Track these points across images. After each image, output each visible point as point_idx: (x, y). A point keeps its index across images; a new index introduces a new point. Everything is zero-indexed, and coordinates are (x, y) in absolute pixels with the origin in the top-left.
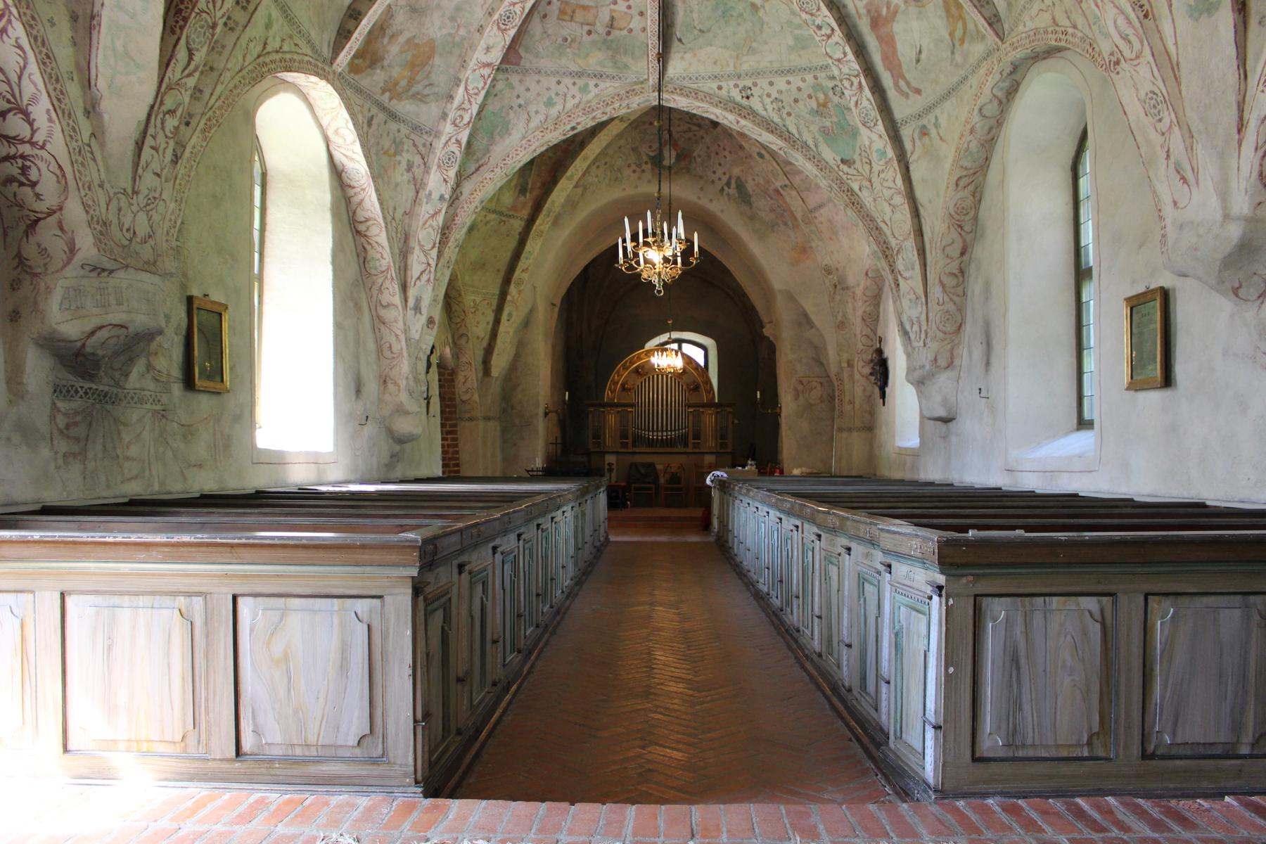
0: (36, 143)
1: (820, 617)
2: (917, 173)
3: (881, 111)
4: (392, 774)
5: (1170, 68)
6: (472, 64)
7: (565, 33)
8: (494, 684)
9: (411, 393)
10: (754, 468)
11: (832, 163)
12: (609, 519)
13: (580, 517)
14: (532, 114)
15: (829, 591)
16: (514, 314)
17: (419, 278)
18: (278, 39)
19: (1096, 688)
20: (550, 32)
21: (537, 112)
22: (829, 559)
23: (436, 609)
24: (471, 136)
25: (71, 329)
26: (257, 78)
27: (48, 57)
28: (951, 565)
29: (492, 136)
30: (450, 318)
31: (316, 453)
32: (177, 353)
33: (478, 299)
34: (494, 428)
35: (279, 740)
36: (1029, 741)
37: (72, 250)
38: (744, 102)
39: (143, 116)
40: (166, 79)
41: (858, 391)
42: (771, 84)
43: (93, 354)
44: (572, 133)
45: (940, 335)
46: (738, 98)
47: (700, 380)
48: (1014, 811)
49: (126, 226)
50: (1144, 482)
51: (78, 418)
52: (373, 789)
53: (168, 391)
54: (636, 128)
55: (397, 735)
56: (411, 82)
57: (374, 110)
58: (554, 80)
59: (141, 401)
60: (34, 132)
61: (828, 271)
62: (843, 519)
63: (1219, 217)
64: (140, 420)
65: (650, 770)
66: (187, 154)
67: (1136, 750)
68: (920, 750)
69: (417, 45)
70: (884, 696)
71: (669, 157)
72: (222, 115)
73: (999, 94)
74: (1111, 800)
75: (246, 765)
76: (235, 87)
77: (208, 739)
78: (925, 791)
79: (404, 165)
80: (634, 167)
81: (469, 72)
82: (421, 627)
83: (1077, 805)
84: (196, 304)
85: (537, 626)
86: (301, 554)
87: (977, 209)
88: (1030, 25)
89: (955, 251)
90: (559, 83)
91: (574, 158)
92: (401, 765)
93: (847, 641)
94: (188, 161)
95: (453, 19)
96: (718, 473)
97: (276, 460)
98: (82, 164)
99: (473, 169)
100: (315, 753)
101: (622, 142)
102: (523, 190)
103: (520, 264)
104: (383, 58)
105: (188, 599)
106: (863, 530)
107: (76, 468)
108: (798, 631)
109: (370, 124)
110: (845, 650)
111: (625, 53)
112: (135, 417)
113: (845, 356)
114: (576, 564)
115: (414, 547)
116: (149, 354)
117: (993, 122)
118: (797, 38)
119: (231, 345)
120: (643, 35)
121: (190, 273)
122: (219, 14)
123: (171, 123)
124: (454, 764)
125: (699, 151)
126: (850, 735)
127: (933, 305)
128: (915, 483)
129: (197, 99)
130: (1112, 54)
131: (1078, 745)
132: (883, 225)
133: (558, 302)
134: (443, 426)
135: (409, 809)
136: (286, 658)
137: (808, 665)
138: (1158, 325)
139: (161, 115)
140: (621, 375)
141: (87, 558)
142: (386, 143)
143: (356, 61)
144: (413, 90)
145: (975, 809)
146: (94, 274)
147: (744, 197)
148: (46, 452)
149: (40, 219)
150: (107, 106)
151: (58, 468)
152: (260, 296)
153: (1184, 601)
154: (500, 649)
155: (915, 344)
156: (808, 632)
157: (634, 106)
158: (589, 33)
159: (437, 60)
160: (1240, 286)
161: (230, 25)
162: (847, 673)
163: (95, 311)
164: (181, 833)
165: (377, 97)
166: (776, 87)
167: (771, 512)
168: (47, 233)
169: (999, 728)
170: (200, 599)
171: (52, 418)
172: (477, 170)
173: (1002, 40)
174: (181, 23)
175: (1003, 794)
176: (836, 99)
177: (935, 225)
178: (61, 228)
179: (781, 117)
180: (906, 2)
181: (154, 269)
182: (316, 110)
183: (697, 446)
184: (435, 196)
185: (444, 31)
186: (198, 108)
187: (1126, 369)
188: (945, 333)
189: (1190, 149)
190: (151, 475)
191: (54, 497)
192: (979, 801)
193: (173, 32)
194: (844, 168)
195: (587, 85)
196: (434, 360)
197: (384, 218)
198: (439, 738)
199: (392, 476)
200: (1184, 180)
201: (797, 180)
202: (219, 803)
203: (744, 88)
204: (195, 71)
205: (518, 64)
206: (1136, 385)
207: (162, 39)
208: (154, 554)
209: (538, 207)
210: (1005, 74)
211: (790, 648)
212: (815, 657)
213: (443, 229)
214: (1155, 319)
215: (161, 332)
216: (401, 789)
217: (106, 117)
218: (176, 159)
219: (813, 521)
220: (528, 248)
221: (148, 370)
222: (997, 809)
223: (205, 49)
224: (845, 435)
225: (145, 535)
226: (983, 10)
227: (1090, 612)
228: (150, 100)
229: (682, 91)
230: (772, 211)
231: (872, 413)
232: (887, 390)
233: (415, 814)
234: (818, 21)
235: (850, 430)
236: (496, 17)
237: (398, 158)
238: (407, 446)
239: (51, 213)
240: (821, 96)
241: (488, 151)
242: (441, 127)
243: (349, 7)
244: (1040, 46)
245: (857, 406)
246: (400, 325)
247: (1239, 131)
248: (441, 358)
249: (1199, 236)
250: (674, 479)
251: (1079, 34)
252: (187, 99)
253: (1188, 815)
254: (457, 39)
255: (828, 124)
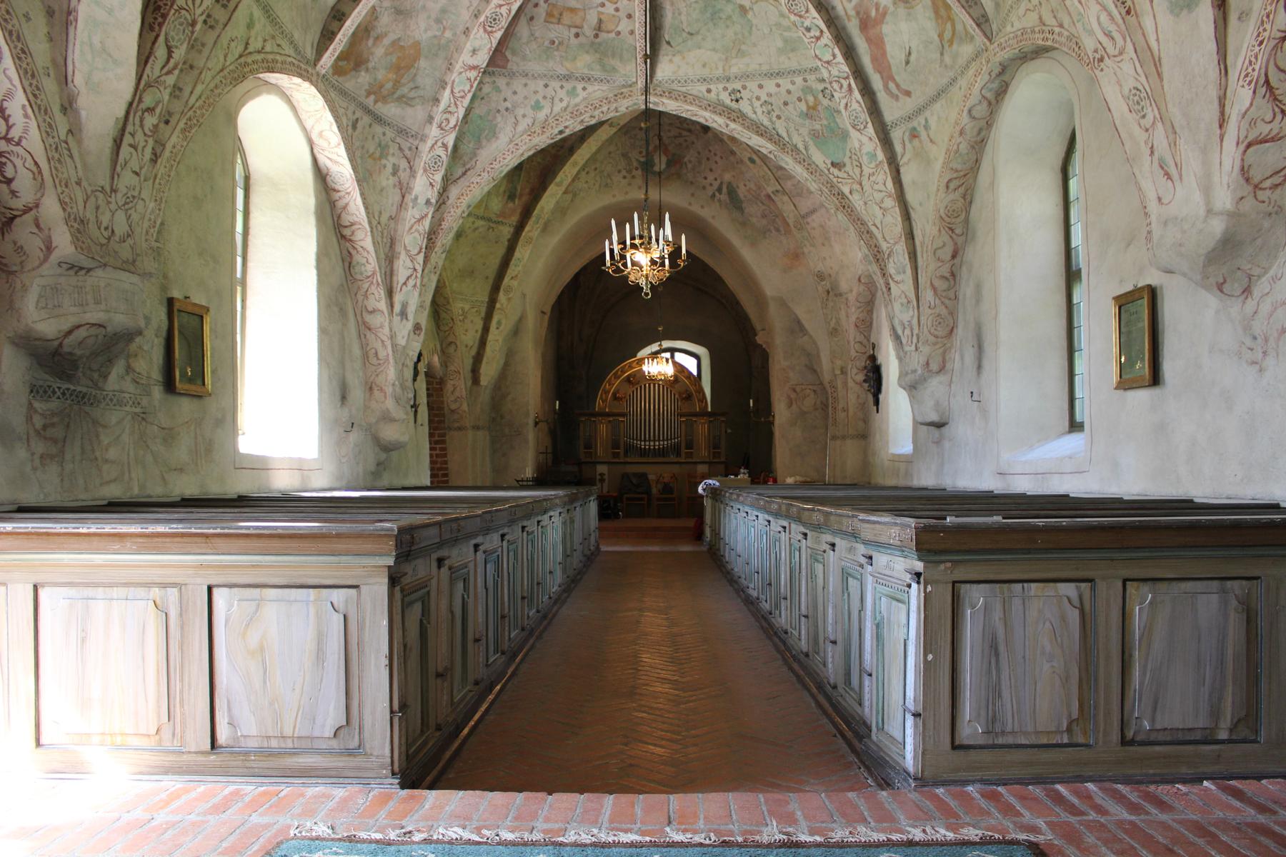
0: (12, 139)
1: (806, 617)
2: (909, 174)
3: (871, 114)
4: (369, 765)
5: (1152, 63)
6: (458, 67)
7: (552, 35)
8: (476, 683)
9: (397, 400)
10: (746, 476)
11: (822, 166)
12: (600, 529)
13: (569, 523)
14: (519, 118)
15: (815, 589)
16: (504, 322)
17: (405, 283)
18: (260, 39)
19: (1075, 672)
20: (537, 34)
21: (524, 116)
22: (815, 557)
23: (416, 600)
24: (457, 139)
25: (49, 328)
26: (238, 78)
27: (24, 52)
28: (929, 551)
29: (479, 141)
30: (438, 327)
31: (300, 460)
32: (157, 355)
33: (467, 304)
34: (483, 437)
35: (254, 732)
36: (1009, 729)
37: (49, 248)
38: (734, 105)
39: (121, 113)
40: (145, 77)
41: (852, 398)
42: (761, 87)
43: (71, 354)
44: (559, 137)
45: (932, 339)
46: (728, 102)
47: (692, 389)
48: (993, 797)
49: (104, 224)
50: (1131, 478)
51: (55, 420)
52: (350, 781)
53: (149, 394)
54: (625, 134)
55: (373, 725)
56: (397, 84)
57: (359, 114)
58: (541, 83)
59: (121, 403)
60: (9, 128)
61: (821, 276)
62: (827, 514)
63: (1202, 212)
64: (120, 422)
65: (631, 765)
66: (167, 154)
67: (1115, 736)
68: (900, 740)
69: (402, 47)
70: (867, 689)
71: (660, 163)
72: (203, 115)
73: (988, 95)
74: (1090, 786)
75: (221, 757)
76: (216, 87)
77: (183, 732)
78: (905, 780)
79: (389, 169)
80: (624, 173)
81: (455, 75)
82: (398, 618)
83: (1057, 792)
84: (177, 306)
85: (523, 629)
86: (276, 544)
87: (968, 213)
88: (1018, 25)
89: (946, 253)
90: (546, 86)
91: (563, 165)
92: (377, 757)
93: (832, 638)
94: (168, 161)
95: (438, 21)
96: (710, 481)
97: (260, 465)
98: (59, 161)
99: (460, 172)
100: (290, 745)
101: (612, 148)
102: (511, 197)
103: (509, 271)
104: (368, 61)
105: (163, 590)
106: (847, 524)
107: (54, 468)
108: (786, 632)
109: (354, 127)
110: (830, 647)
111: (613, 56)
112: (114, 420)
113: (839, 363)
114: (564, 570)
115: (389, 536)
116: (128, 356)
117: (983, 123)
118: (786, 41)
119: (212, 348)
120: (631, 37)
121: (171, 274)
122: (199, 11)
123: (150, 121)
124: (434, 753)
125: (690, 157)
126: (834, 731)
127: (925, 311)
128: (910, 488)
129: (177, 97)
130: (1096, 51)
131: (1058, 732)
132: (873, 229)
133: (548, 309)
134: (431, 435)
135: (384, 799)
136: (262, 649)
137: (796, 666)
138: (1145, 323)
139: (140, 113)
140: (612, 385)
141: (61, 549)
142: (371, 147)
143: (341, 63)
144: (398, 93)
145: (955, 796)
146: (72, 272)
147: (735, 202)
148: (22, 453)
149: (15, 217)
150: (83, 102)
151: (34, 469)
152: (243, 301)
153: (1163, 586)
154: (483, 648)
155: (907, 348)
156: (796, 633)
157: (623, 109)
158: (577, 35)
159: (422, 63)
160: (1225, 281)
161: (209, 23)
162: (832, 669)
163: (73, 309)
164: (154, 823)
165: (362, 99)
166: (765, 90)
167: (761, 516)
168: (23, 232)
169: (979, 715)
170: (175, 590)
171: (29, 419)
172: (464, 174)
173: (990, 40)
174: (160, 20)
175: (983, 781)
176: (825, 102)
177: (926, 228)
178: (38, 226)
179: (771, 120)
180: (895, 3)
181: (133, 269)
182: (300, 112)
183: (690, 455)
184: (422, 201)
185: (430, 34)
186: (177, 106)
187: (1115, 369)
188: (936, 337)
189: (1173, 144)
190: (130, 479)
191: (30, 498)
192: (958, 788)
193: (152, 29)
194: (836, 171)
195: (574, 88)
196: (422, 368)
197: (370, 223)
198: (418, 731)
199: (378, 484)
200: (1168, 176)
201: (788, 185)
202: (193, 795)
203: (734, 91)
204: (174, 68)
205: (504, 67)
206: (1126, 383)
207: (140, 35)
208: (128, 545)
209: (526, 213)
210: (993, 75)
211: (778, 650)
212: (802, 657)
213: (429, 234)
214: (1143, 316)
215: (140, 333)
216: (378, 781)
217: (83, 113)
218: (155, 158)
219: (799, 520)
220: (517, 254)
221: (128, 373)
222: (977, 796)
223: (185, 46)
224: (838, 442)
225: (119, 526)
226: (971, 11)
227: (1069, 599)
228: (128, 96)
229: (671, 94)
230: (764, 216)
231: (866, 420)
232: (881, 397)
233: (391, 804)
234: (807, 23)
235: (844, 438)
236: (482, 19)
237: (384, 161)
238: (394, 454)
239: (27, 210)
240: (811, 99)
241: (475, 155)
242: (427, 131)
243: (333, 8)
244: (1028, 45)
245: (851, 413)
246: (386, 330)
247: (1221, 126)
248: (429, 366)
249: (1184, 232)
250: (667, 489)
251: (1066, 33)
252: (166, 97)
253: (1165, 798)
254: (443, 41)
255: (818, 127)
